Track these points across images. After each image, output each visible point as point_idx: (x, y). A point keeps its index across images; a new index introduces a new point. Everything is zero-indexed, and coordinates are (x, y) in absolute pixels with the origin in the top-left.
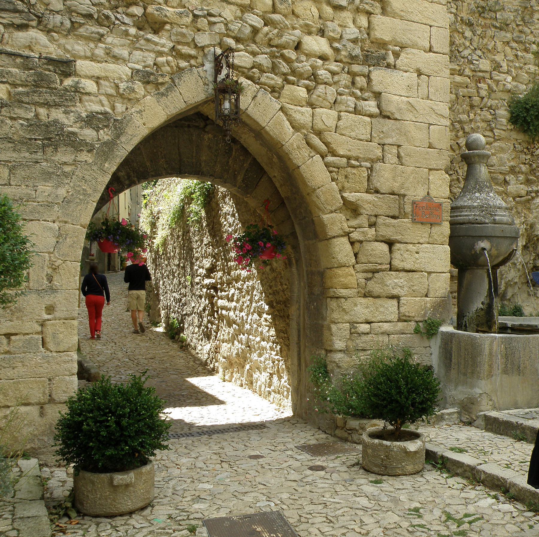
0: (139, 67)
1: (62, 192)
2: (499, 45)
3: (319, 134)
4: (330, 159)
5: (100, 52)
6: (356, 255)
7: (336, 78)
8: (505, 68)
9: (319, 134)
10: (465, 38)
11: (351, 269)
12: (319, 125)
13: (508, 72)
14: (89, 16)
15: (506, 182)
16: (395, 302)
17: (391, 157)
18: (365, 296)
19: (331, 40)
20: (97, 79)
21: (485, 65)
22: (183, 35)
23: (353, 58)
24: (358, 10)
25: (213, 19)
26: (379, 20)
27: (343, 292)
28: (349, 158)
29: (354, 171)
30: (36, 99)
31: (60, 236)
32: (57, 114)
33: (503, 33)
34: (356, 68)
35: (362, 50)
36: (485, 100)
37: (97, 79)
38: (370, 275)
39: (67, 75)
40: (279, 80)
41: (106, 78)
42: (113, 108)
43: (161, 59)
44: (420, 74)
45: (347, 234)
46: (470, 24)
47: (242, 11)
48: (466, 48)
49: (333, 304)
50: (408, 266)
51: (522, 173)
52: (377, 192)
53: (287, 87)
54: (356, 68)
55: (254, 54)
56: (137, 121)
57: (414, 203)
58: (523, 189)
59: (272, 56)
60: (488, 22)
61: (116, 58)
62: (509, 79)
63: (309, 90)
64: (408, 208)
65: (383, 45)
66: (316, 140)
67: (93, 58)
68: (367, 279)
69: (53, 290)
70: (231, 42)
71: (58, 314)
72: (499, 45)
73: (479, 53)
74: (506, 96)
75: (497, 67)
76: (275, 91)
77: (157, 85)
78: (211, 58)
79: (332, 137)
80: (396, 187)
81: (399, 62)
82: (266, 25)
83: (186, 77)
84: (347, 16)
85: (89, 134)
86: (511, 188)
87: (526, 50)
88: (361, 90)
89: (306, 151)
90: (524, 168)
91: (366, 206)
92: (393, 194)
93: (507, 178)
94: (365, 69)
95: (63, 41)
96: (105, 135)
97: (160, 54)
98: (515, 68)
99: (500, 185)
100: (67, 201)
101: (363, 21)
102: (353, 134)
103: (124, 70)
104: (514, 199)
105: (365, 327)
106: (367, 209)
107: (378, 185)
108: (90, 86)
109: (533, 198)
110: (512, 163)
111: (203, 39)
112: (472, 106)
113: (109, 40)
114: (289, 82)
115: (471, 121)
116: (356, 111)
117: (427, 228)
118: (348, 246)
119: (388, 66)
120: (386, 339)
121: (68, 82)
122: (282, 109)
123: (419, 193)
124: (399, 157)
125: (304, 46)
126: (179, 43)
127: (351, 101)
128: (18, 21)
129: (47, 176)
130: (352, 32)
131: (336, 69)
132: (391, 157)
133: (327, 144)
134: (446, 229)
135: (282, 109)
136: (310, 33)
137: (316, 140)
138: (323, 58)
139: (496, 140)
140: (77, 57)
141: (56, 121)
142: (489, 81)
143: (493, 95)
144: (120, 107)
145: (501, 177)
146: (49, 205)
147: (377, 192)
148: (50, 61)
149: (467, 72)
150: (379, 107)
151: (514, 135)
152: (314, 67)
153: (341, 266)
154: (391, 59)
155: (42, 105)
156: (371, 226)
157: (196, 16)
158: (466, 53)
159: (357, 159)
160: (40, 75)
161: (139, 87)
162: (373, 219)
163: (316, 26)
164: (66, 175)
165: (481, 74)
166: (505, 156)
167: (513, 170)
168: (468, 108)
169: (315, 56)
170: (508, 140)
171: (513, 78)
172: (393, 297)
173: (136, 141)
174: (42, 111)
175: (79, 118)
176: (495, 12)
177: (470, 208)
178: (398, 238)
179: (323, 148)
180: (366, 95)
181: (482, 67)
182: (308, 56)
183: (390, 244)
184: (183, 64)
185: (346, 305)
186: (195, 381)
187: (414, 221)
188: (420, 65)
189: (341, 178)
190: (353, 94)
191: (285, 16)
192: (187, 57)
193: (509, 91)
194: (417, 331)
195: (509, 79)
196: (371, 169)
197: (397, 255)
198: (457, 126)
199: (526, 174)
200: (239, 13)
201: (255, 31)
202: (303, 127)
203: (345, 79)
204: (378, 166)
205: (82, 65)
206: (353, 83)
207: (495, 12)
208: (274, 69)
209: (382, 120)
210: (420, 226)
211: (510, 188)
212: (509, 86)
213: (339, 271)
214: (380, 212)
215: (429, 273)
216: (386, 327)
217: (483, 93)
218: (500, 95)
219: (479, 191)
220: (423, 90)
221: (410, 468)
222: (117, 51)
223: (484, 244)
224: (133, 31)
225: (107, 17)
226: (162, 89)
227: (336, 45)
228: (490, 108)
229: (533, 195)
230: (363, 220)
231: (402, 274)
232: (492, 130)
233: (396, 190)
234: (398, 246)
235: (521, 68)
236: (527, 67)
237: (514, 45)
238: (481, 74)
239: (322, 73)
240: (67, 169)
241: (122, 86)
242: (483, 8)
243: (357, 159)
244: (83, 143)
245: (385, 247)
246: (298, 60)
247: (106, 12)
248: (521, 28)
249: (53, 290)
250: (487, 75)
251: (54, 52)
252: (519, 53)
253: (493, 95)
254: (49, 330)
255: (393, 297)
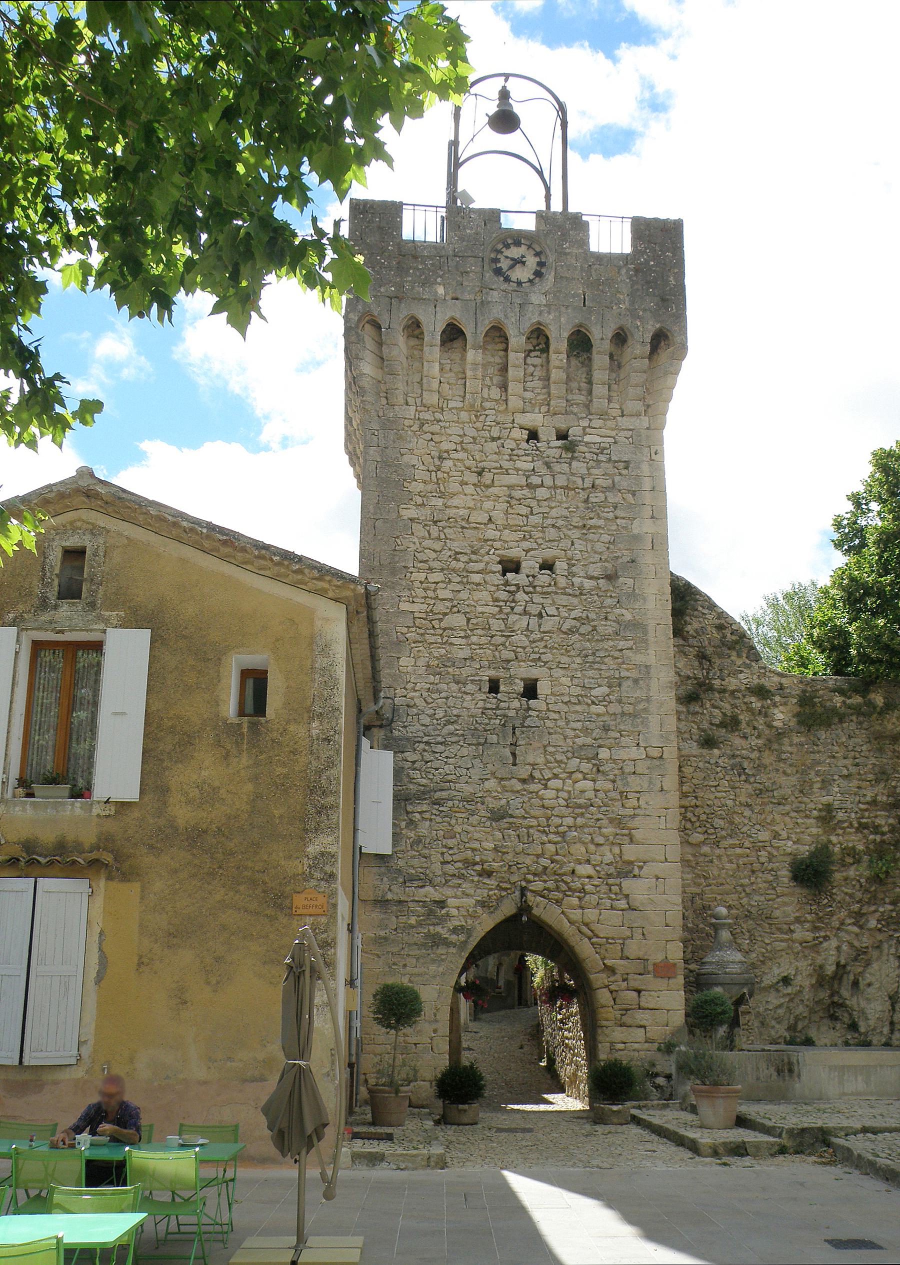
0: (479, 898)
1: (441, 969)
2: (778, 818)
3: (587, 925)
4: (594, 940)
5: (459, 893)
6: (614, 1000)
7: (598, 889)
8: (784, 834)
9: (587, 925)
10: (745, 817)
11: (611, 1009)
12: (586, 920)
13: (788, 838)
14: (454, 875)
15: (792, 931)
16: (642, 1030)
17: (638, 936)
18: (621, 1026)
19: (594, 866)
20: (458, 908)
21: (764, 836)
22: (503, 878)
23: (609, 876)
24: (613, 844)
25: (519, 866)
26: (627, 848)
27: (604, 1023)
28: (607, 938)
29: (611, 946)
30: (429, 922)
31: (440, 992)
32: (438, 929)
33: (781, 807)
34: (611, 881)
35: (616, 868)
36: (766, 864)
37: (458, 908)
38: (624, 1012)
39: (443, 908)
40: (561, 895)
41: (462, 907)
42: (466, 922)
43: (491, 893)
44: (658, 878)
45: (607, 986)
46: (748, 805)
47: (538, 858)
48: (745, 825)
49: (599, 1031)
50: (651, 1006)
51: (808, 922)
52: (628, 958)
53: (566, 898)
54: (611, 881)
55: (545, 882)
56: (479, 928)
57: (654, 964)
58: (809, 936)
59: (556, 881)
60: (767, 800)
61: (468, 895)
62: (790, 843)
63: (580, 899)
64: (651, 968)
65: (631, 863)
66: (585, 929)
67: (455, 897)
68: (622, 1015)
69: (436, 1021)
70: (530, 877)
71: (439, 1034)
72: (778, 818)
73: (758, 827)
74: (788, 859)
75: (776, 836)
76: (558, 902)
77: (489, 907)
78: (519, 888)
79: (595, 927)
80: (641, 954)
81: (642, 873)
82: (552, 862)
83: (505, 901)
84: (605, 849)
85: (454, 938)
86: (797, 936)
87: (807, 817)
88: (616, 894)
89: (578, 937)
90: (809, 917)
91: (621, 968)
92: (639, 959)
93: (792, 927)
94: (618, 881)
95: (441, 890)
96: (462, 938)
97: (491, 889)
98: (796, 833)
99: (786, 933)
100: (443, 974)
101: (616, 850)
102: (610, 923)
103: (472, 901)
104: (801, 944)
105: (622, 1046)
106: (620, 970)
107: (628, 955)
108: (454, 912)
109: (821, 943)
110: (797, 914)
111: (514, 878)
112: (753, 872)
113: (464, 886)
114: (567, 896)
115: (752, 883)
116: (612, 908)
117: (665, 981)
118: (608, 994)
119: (635, 876)
120: (636, 1054)
121: (444, 911)
122: (563, 913)
123: (660, 957)
124: (643, 934)
125: (576, 872)
126: (501, 882)
127: (608, 903)
128: (421, 884)
129: (434, 961)
130: (609, 858)
131: (597, 883)
132: (638, 936)
133: (592, 931)
134: (681, 980)
135: (563, 913)
136: (580, 864)
137: (585, 929)
138: (589, 877)
139: (778, 897)
140: (447, 898)
141: (438, 933)
142: (769, 849)
143: (774, 860)
144: (470, 921)
145: (785, 926)
146: (434, 977)
147: (628, 958)
148: (435, 902)
149: (747, 844)
150: (628, 904)
151: (798, 890)
152: (583, 885)
153: (603, 1007)
154: (636, 872)
155: (431, 925)
156: (624, 980)
157: (510, 866)
158: (745, 829)
159: (613, 939)
160: (431, 910)
161: (479, 910)
162: (625, 976)
163: (583, 859)
164: (443, 960)
165: (761, 844)
166: (788, 909)
167: (798, 920)
168: (750, 873)
169: (584, 877)
170: (792, 895)
171: (794, 842)
172: (641, 1027)
173: (478, 939)
174: (431, 928)
175: (449, 930)
176: (772, 791)
177: (711, 963)
178: (644, 987)
179: (590, 933)
180: (619, 897)
181: (760, 838)
182: (579, 877)
183: (639, 992)
184: (504, 893)
185: (607, 1031)
186: (545, 1096)
187: (655, 976)
188: (657, 873)
189: (603, 951)
190: (610, 898)
191: (564, 856)
192: (506, 889)
193: (791, 854)
194: (659, 1050)
195: (790, 843)
196: (623, 944)
197: (643, 999)
198: (739, 889)
199: (813, 922)
200: (535, 859)
201: (545, 868)
202: (576, 922)
203: (604, 888)
204: (627, 942)
205: (451, 902)
206: (610, 890)
207: (772, 791)
208: (557, 889)
209: (630, 912)
210: (660, 979)
211: (795, 936)
212: (789, 850)
213: (602, 1010)
214: (629, 971)
215: (668, 1010)
216: (636, 1046)
217: (763, 860)
218: (780, 858)
219: (719, 950)
220: (661, 888)
221: (615, 1120)
222: (468, 892)
223: (718, 990)
224: (476, 879)
225: (463, 875)
226: (492, 909)
227: (598, 868)
228: (772, 870)
229: (821, 940)
230: (618, 977)
231: (647, 1011)
232: (774, 888)
233: (641, 957)
234: (643, 993)
235: (803, 832)
236: (808, 831)
237: (793, 814)
238: (761, 844)
239: (588, 888)
240: (443, 957)
241: (471, 910)
242: (760, 790)
243: (613, 939)
244: (451, 943)
245: (635, 994)
246: (573, 881)
247: (462, 871)
248: (800, 799)
249: (436, 1021)
250: (768, 844)
251: (437, 897)
252: (799, 821)
253: (774, 860)
254: (435, 1042)
255: (641, 1027)
